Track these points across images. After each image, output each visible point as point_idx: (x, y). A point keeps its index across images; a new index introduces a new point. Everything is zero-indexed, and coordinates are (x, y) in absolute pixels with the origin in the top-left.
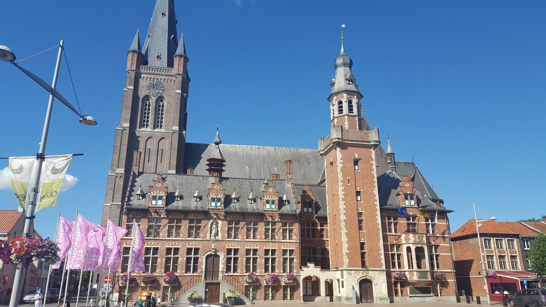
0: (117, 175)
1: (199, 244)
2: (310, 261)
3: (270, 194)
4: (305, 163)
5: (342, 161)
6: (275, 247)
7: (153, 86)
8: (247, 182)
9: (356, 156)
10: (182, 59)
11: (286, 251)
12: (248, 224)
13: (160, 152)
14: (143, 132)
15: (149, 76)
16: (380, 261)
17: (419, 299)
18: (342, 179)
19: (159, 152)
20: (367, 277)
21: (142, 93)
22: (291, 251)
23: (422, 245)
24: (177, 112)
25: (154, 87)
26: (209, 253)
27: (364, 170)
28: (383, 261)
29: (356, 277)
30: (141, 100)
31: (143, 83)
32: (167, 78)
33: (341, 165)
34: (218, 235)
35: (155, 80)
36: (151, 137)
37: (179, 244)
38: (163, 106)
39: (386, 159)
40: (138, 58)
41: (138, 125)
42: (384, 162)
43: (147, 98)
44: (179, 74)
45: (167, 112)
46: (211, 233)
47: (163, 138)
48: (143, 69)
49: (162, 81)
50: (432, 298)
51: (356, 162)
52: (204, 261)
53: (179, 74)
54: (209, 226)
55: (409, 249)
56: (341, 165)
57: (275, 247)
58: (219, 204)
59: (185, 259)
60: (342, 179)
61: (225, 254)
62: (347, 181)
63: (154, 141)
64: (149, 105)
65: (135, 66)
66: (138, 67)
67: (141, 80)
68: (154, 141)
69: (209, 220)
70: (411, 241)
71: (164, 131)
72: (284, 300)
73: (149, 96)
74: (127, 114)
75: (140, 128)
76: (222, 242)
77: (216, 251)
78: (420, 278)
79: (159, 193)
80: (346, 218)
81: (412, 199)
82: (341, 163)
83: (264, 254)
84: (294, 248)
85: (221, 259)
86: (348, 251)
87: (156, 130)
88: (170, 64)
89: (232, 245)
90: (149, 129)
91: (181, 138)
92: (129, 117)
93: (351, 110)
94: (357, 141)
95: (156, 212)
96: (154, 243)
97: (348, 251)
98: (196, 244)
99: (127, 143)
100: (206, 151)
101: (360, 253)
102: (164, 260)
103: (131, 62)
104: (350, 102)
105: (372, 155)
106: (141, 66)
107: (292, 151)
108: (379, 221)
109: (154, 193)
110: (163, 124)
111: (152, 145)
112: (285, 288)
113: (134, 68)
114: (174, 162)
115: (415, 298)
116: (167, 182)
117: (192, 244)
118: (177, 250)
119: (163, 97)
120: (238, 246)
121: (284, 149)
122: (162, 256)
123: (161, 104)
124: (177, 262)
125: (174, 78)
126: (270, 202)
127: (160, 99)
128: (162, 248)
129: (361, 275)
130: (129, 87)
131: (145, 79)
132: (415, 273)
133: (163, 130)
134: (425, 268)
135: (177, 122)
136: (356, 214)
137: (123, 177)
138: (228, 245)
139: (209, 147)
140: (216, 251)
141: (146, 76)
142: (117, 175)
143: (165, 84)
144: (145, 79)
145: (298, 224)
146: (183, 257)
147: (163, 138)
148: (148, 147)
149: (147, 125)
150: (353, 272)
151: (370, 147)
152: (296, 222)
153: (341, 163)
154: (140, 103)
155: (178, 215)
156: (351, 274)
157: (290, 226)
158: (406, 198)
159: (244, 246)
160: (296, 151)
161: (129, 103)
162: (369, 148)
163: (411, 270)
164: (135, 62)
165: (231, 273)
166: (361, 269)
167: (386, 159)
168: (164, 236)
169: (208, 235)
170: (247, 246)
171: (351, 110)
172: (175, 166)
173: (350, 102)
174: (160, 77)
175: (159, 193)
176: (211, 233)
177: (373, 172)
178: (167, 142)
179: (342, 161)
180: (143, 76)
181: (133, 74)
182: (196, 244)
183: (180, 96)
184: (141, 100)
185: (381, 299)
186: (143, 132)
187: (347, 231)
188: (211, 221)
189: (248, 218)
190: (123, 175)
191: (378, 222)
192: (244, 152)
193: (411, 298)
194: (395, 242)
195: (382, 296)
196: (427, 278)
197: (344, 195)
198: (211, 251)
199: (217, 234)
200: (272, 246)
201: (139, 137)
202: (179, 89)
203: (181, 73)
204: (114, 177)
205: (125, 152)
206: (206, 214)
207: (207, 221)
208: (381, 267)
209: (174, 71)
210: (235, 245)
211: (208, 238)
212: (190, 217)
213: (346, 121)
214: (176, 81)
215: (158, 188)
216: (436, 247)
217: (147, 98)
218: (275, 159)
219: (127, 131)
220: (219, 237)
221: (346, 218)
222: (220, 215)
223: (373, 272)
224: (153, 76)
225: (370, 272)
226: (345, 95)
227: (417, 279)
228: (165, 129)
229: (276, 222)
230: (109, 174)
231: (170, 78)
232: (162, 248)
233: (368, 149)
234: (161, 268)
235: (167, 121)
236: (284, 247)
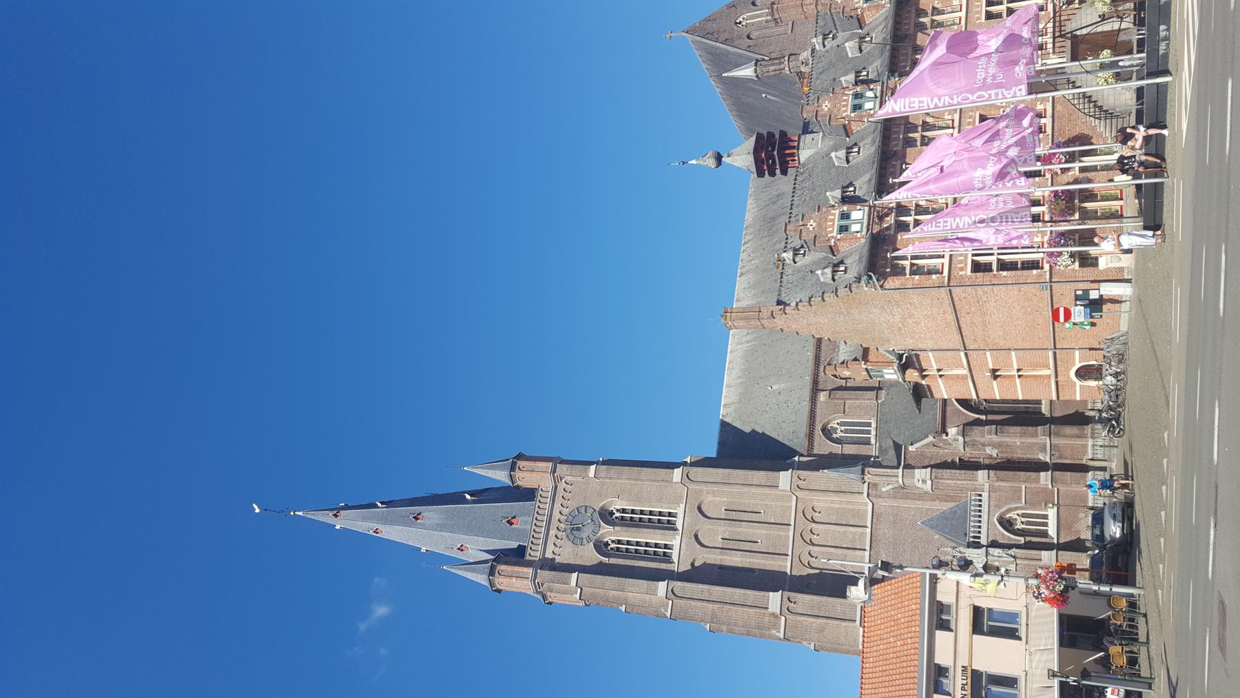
0: (785, 608)
4: (779, 203)
7: (574, 530)
10: (521, 463)
11: (990, 16)
12: (922, 28)
13: (734, 515)
14: (681, 553)
15: (552, 539)
19: (734, 516)
21: (590, 556)
25: (578, 529)
30: (605, 560)
31: (565, 552)
32: (559, 500)
35: (562, 526)
36: (696, 537)
38: (624, 511)
40: (506, 563)
41: (663, 566)
43: (601, 547)
44: (554, 471)
45: (638, 500)
47: (699, 509)
48: (534, 554)
53: (554, 471)
63: (705, 528)
64: (619, 542)
65: (525, 570)
66: (529, 564)
67: (558, 559)
68: (705, 528)
71: (682, 506)
74: (636, 591)
87: (679, 525)
88: (529, 494)
90: (675, 542)
91: (705, 463)
92: (643, 583)
95: (881, 218)
99: (706, 587)
100: (738, 424)
103: (516, 581)
106: (528, 557)
107: (749, 237)
111: (715, 533)
112: (1086, 215)
113: (530, 571)
114: (759, 476)
119: (602, 509)
121: (743, 256)
125: (562, 485)
127: (606, 516)
130: (573, 583)
131: (557, 550)
133: (680, 511)
137: (792, 594)
139: (728, 420)
141: (550, 548)
142: (785, 608)
143: (573, 505)
144: (557, 550)
147: (699, 509)
154: (613, 561)
157: (926, 14)
160: (751, 230)
161: (608, 586)
164: (516, 569)
170: (979, 18)
172: (770, 473)
174: (556, 515)
178: (710, 498)
180: (549, 555)
181: (544, 575)
184: (605, 560)
186: (681, 553)
190: (787, 594)
192: (744, 339)
201: (692, 564)
202: (586, 471)
204: (790, 617)
205: (729, 590)
212: (900, 148)
214: (569, 479)
215: (819, 225)
217: (601, 547)
218: (764, 271)
219: (678, 585)
224: (553, 532)
228: (677, 502)
230: (781, 636)
231: (560, 492)
235: (660, 500)
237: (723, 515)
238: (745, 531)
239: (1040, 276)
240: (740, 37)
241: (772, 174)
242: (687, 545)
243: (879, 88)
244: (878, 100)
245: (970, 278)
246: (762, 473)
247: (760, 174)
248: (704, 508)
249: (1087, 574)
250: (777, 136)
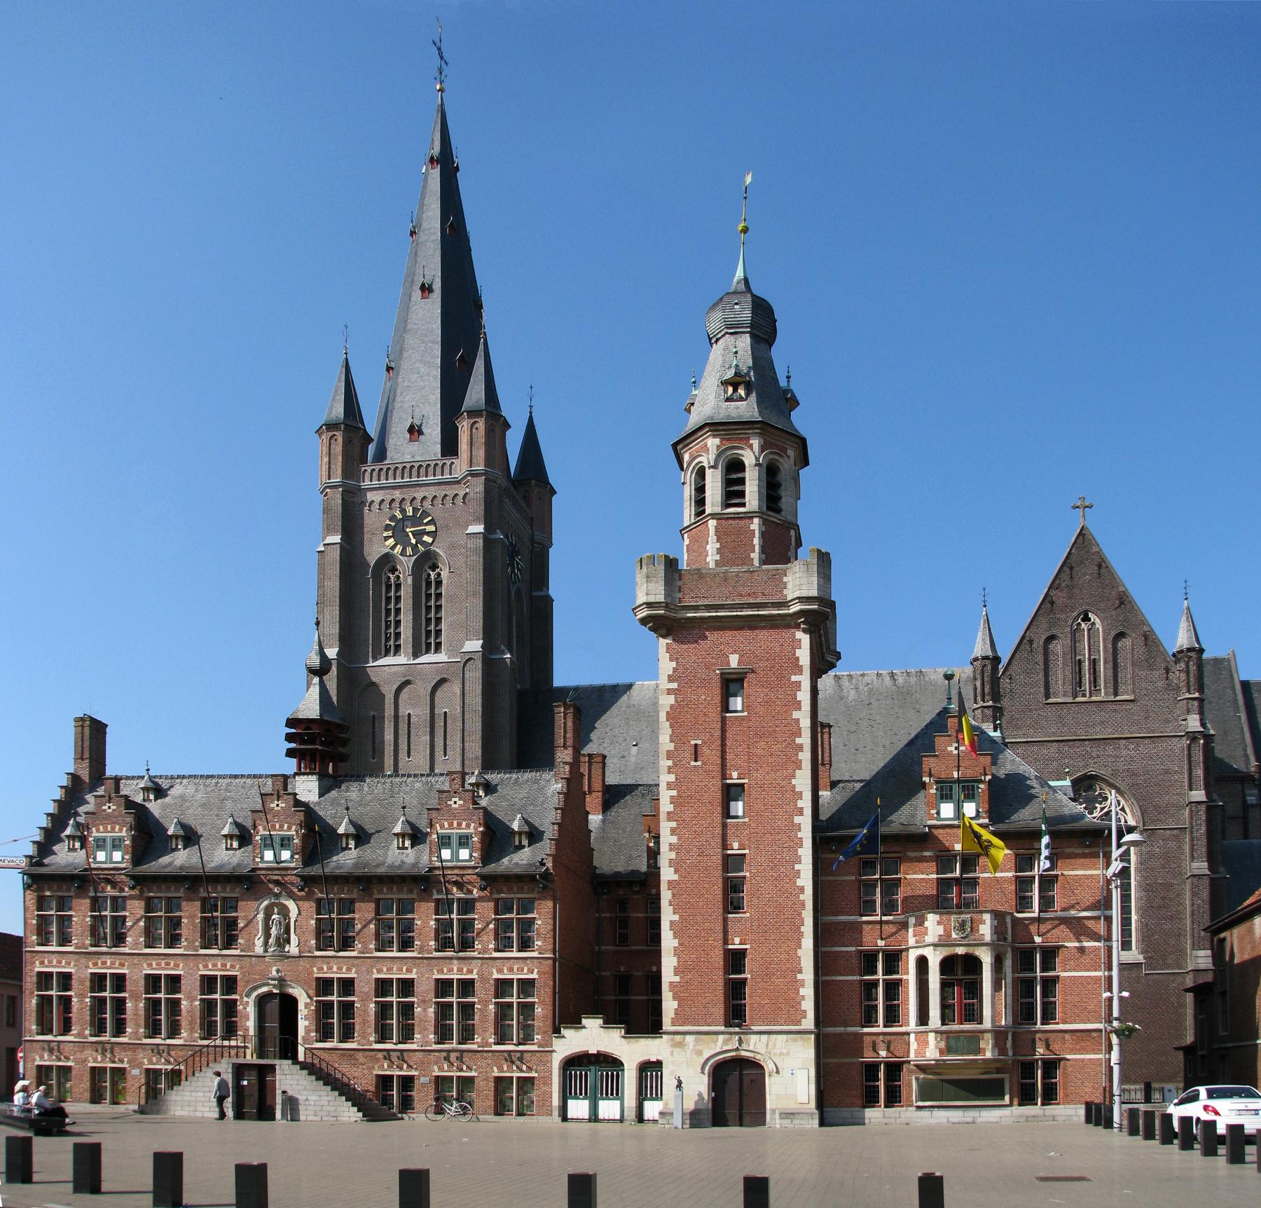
1: (233, 966)
2: (593, 1012)
3: (453, 814)
5: (674, 685)
6: (470, 971)
8: (417, 785)
9: (734, 661)
13: (439, 724)
14: (387, 668)
16: (795, 1003)
17: (956, 1116)
18: (671, 747)
20: (744, 1053)
22: (527, 986)
23: (970, 950)
24: (474, 594)
26: (265, 989)
27: (761, 710)
28: (808, 1005)
29: (699, 1053)
31: (374, 520)
32: (440, 492)
33: (671, 699)
34: (288, 941)
36: (407, 683)
37: (177, 966)
39: (1167, 670)
42: (1161, 684)
43: (387, 561)
44: (473, 474)
46: (267, 935)
49: (427, 504)
50: (1006, 1112)
51: (731, 683)
52: (251, 1010)
53: (473, 474)
54: (261, 916)
55: (922, 962)
56: (671, 699)
57: (470, 971)
58: (286, 855)
59: (197, 1003)
60: (671, 747)
61: (312, 992)
62: (689, 754)
64: (398, 586)
69: (258, 897)
70: (931, 938)
72: (497, 1114)
73: (393, 556)
75: (375, 659)
76: (301, 962)
77: (282, 981)
78: (949, 1050)
79: (113, 830)
80: (676, 877)
81: (970, 797)
82: (669, 692)
83: (433, 994)
84: (535, 976)
85: (301, 1006)
86: (677, 979)
89: (331, 968)
90: (402, 659)
93: (733, 493)
94: (741, 607)
96: (113, 963)
97: (677, 979)
98: (224, 965)
101: (721, 983)
102: (142, 1005)
104: (734, 468)
105: (798, 653)
108: (806, 879)
109: (98, 831)
110: (443, 638)
115: (937, 1113)
116: (167, 799)
117: (215, 965)
118: (174, 981)
119: (435, 554)
120: (349, 970)
122: (136, 997)
123: (433, 574)
124: (179, 1013)
126: (455, 841)
128: (136, 974)
129: (721, 1045)
130: (330, 540)
131: (459, 500)
132: (932, 1036)
133: (442, 657)
134: (981, 1023)
135: (478, 624)
136: (718, 859)
138: (320, 969)
140: (282, 981)
143: (437, 512)
144: (459, 500)
145: (550, 904)
146: (192, 1000)
147: (407, 683)
148: (404, 711)
149: (398, 648)
150: (689, 1038)
151: (787, 623)
152: (545, 898)
153: (669, 692)
155: (168, 889)
156: (681, 1045)
158: (945, 796)
159: (370, 972)
162: (788, 626)
163: (923, 1028)
165: (106, 1037)
166: (722, 1028)
167: (1167, 670)
168: (137, 944)
169: (259, 943)
170: (379, 971)
171: (733, 493)
173: (734, 468)
174: (419, 494)
175: (113, 830)
176: (267, 935)
177: (796, 715)
179: (674, 685)
180: (370, 496)
182: (224, 965)
183: (480, 542)
185: (788, 1115)
186: (387, 668)
187: (676, 917)
188: (266, 903)
189: (380, 892)
191: (799, 882)
193: (925, 1113)
194: (881, 943)
195: (791, 1106)
196: (978, 1051)
197: (673, 800)
198: (268, 984)
199: (284, 940)
200: (460, 970)
202: (476, 521)
203: (480, 467)
206: (249, 883)
207: (254, 904)
208: (798, 1023)
209: (460, 466)
210: (340, 969)
211: (259, 950)
213: (712, 536)
216: (1050, 955)
220: (293, 948)
221: (676, 877)
222: (292, 884)
223: (764, 1037)
224: (397, 494)
225: (754, 1038)
226: (713, 443)
227: (937, 1055)
228: (450, 652)
229: (474, 900)
231: (451, 491)
232: (136, 974)
233: (786, 634)
234: (138, 1026)
236: (500, 971)
237: (439, 711)
238: (421, 740)
239: (30, 1031)
240: (1052, 624)
241: (289, 738)
242: (395, 674)
243: (293, 865)
244: (275, 865)
245: (32, 971)
246: (479, 752)
247: (291, 723)
248: (445, 687)
249: (1255, 1166)
250: (293, 745)
